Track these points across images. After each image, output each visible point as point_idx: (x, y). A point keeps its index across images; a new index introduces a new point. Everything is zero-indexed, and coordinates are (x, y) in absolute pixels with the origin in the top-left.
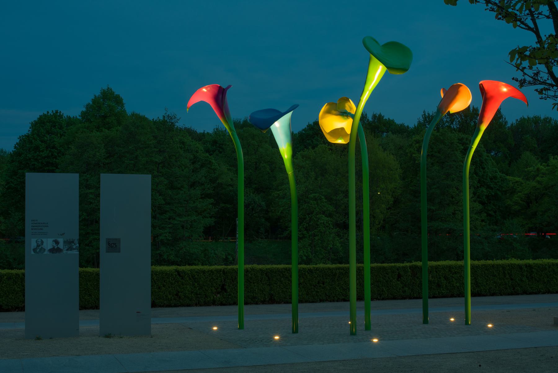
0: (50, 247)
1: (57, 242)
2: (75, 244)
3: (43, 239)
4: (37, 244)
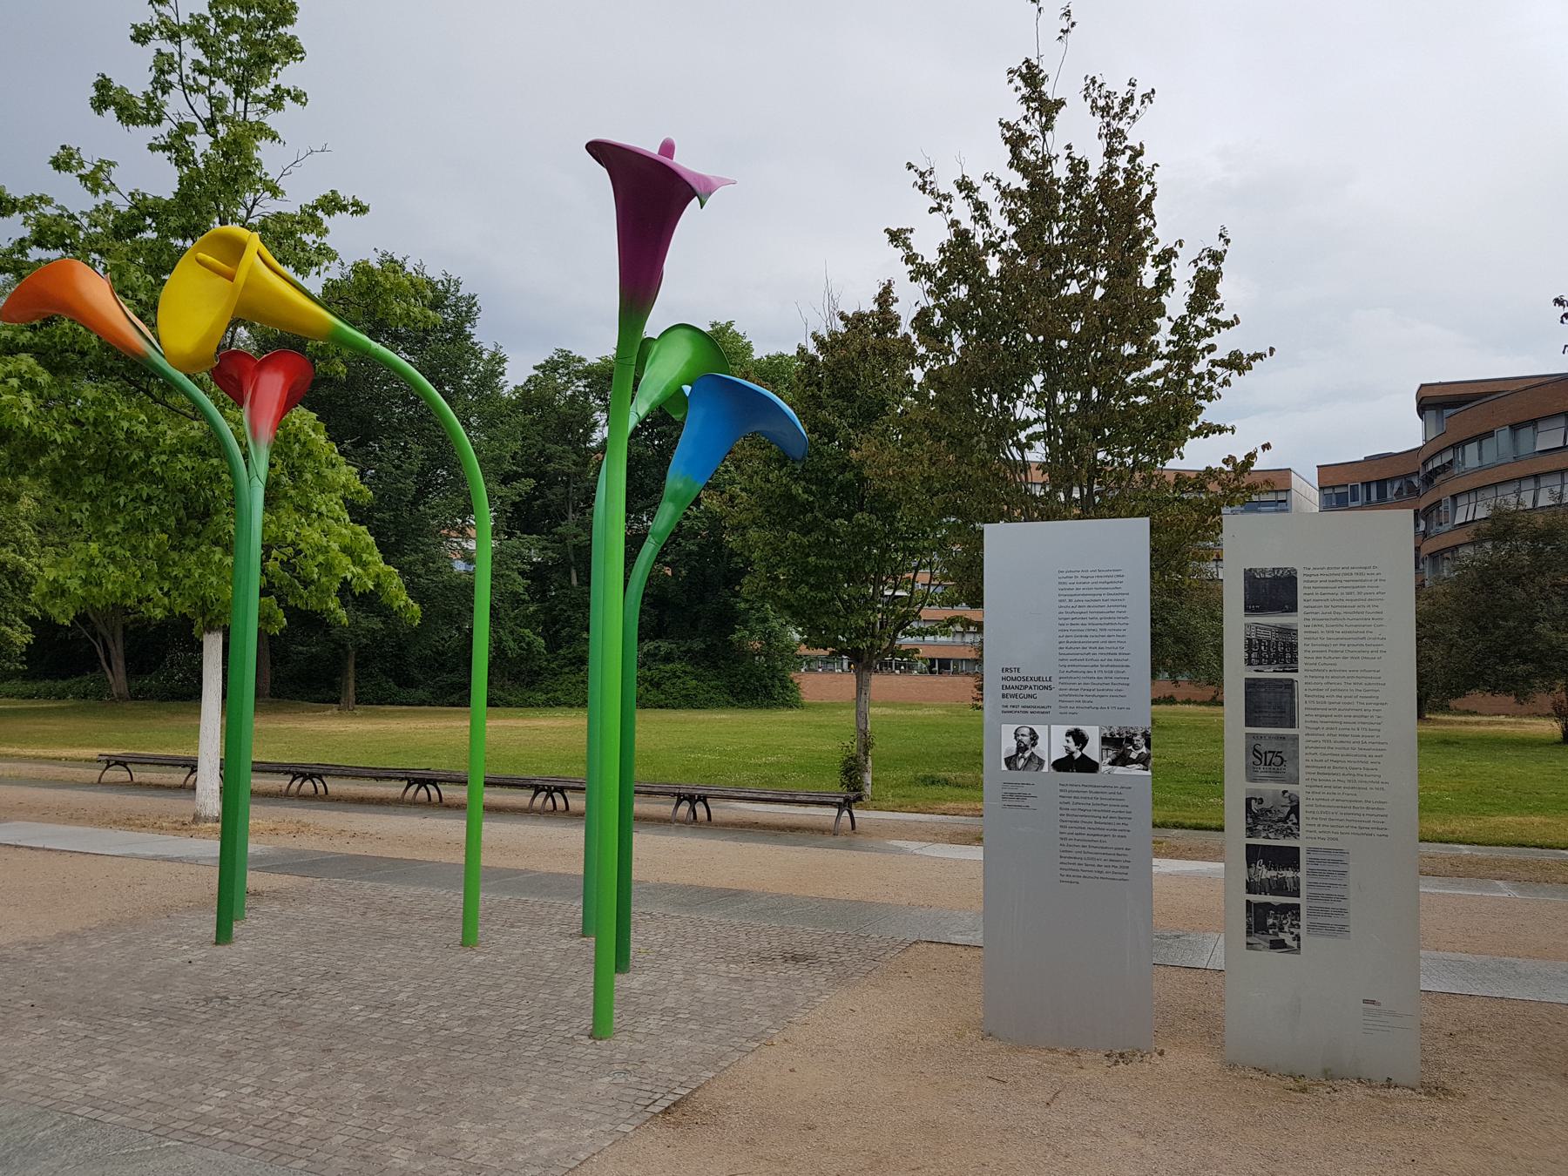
0: (1059, 753)
1: (1079, 738)
2: (1136, 748)
3: (1035, 728)
4: (1019, 742)
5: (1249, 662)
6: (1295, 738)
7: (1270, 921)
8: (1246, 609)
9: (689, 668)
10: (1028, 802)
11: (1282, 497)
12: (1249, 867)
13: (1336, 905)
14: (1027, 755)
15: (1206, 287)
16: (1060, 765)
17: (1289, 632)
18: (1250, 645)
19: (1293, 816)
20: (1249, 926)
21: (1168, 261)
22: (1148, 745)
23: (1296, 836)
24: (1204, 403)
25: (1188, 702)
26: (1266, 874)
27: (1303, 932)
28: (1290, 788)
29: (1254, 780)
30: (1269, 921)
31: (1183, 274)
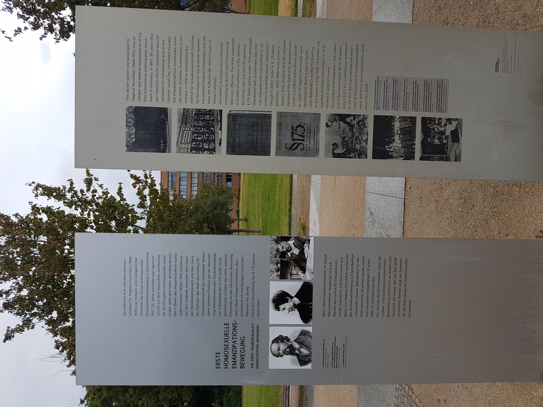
0: (295, 317)
1: (281, 299)
2: (289, 249)
3: (272, 337)
4: (285, 353)
5: (212, 151)
6: (280, 115)
7: (437, 142)
8: (164, 151)
9: (226, 395)
10: (339, 345)
11: (170, 174)
12: (391, 157)
13: (421, 88)
14: (296, 346)
15: (49, 192)
16: (306, 316)
17: (185, 117)
18: (197, 149)
19: (348, 120)
20: (440, 159)
21: (38, 208)
22: (287, 239)
23: (365, 118)
24: (109, 196)
25: (238, 206)
26: (397, 144)
27: (444, 116)
28: (323, 121)
29: (317, 151)
30: (439, 142)
31: (44, 202)
